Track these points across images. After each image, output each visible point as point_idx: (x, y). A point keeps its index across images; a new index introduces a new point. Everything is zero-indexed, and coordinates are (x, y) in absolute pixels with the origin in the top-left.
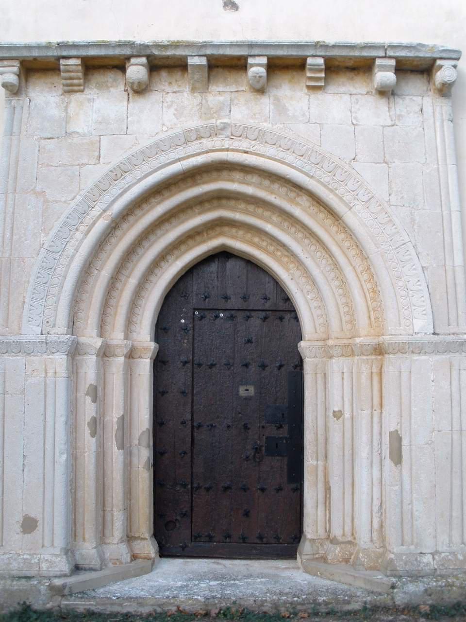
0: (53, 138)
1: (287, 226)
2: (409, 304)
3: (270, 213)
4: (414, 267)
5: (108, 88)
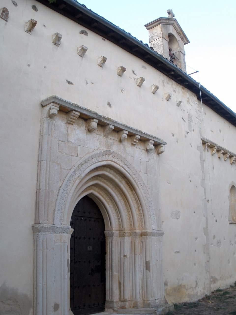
0: (63, 141)
5: (80, 126)
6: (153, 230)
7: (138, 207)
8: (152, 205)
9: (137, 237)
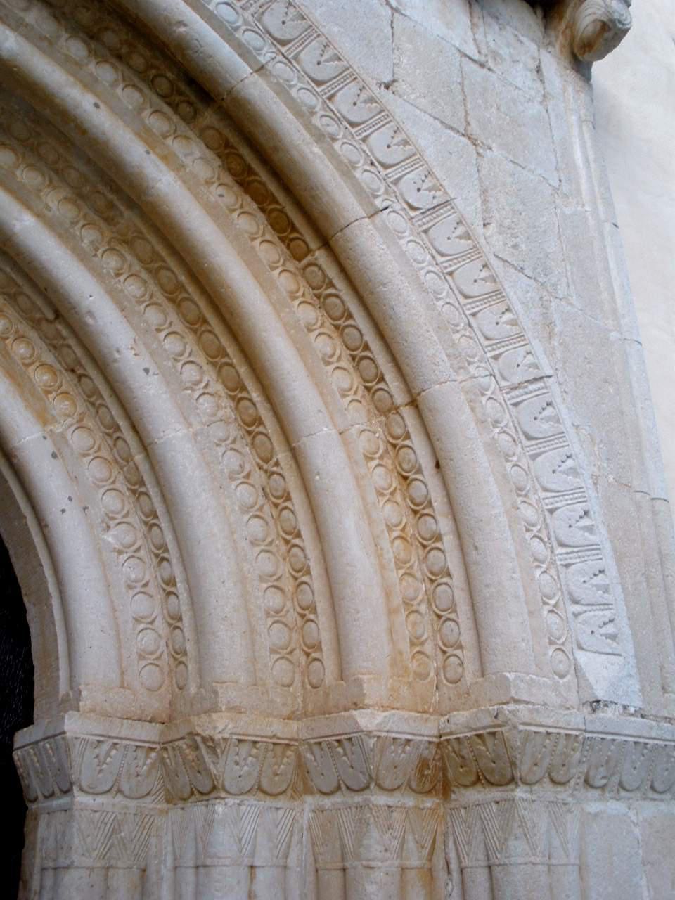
1: (92, 242)
2: (559, 593)
3: (40, 179)
4: (570, 463)
6: (596, 704)
7: (395, 445)
8: (557, 420)
9: (380, 799)
